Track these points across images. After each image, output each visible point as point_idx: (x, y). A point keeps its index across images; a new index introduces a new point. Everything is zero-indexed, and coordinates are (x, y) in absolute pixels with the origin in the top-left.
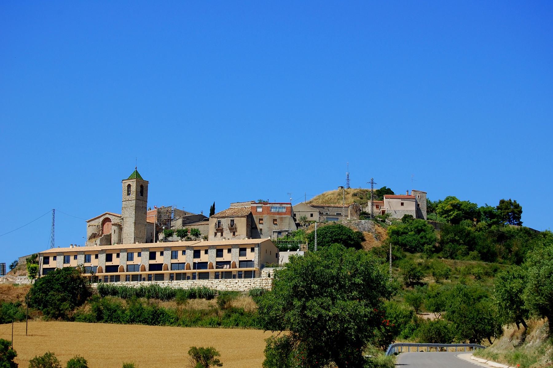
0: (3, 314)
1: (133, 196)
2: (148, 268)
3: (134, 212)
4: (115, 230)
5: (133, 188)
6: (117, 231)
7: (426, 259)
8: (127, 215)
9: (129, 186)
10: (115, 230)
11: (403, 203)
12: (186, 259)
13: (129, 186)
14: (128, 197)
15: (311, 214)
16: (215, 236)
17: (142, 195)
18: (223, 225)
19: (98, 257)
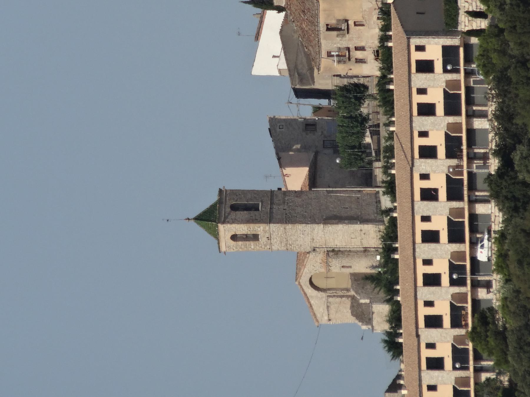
0: (493, 293)
1: (260, 229)
2: (458, 245)
3: (300, 227)
4: (343, 267)
5: (242, 229)
6: (346, 262)
7: (496, 215)
8: (308, 239)
9: (234, 238)
10: (343, 267)
11: (417, 89)
12: (439, 173)
13: (234, 238)
14: (263, 240)
15: (436, 190)
16: (365, 62)
17: (255, 208)
18: (339, 46)
19: (280, 188)
